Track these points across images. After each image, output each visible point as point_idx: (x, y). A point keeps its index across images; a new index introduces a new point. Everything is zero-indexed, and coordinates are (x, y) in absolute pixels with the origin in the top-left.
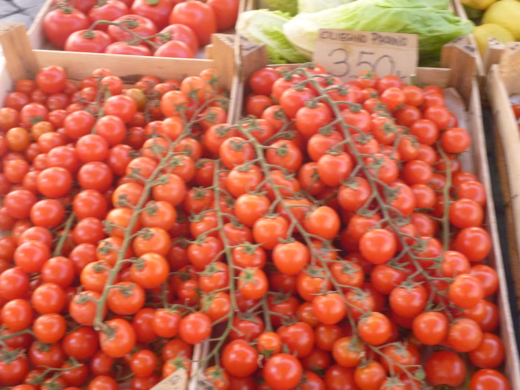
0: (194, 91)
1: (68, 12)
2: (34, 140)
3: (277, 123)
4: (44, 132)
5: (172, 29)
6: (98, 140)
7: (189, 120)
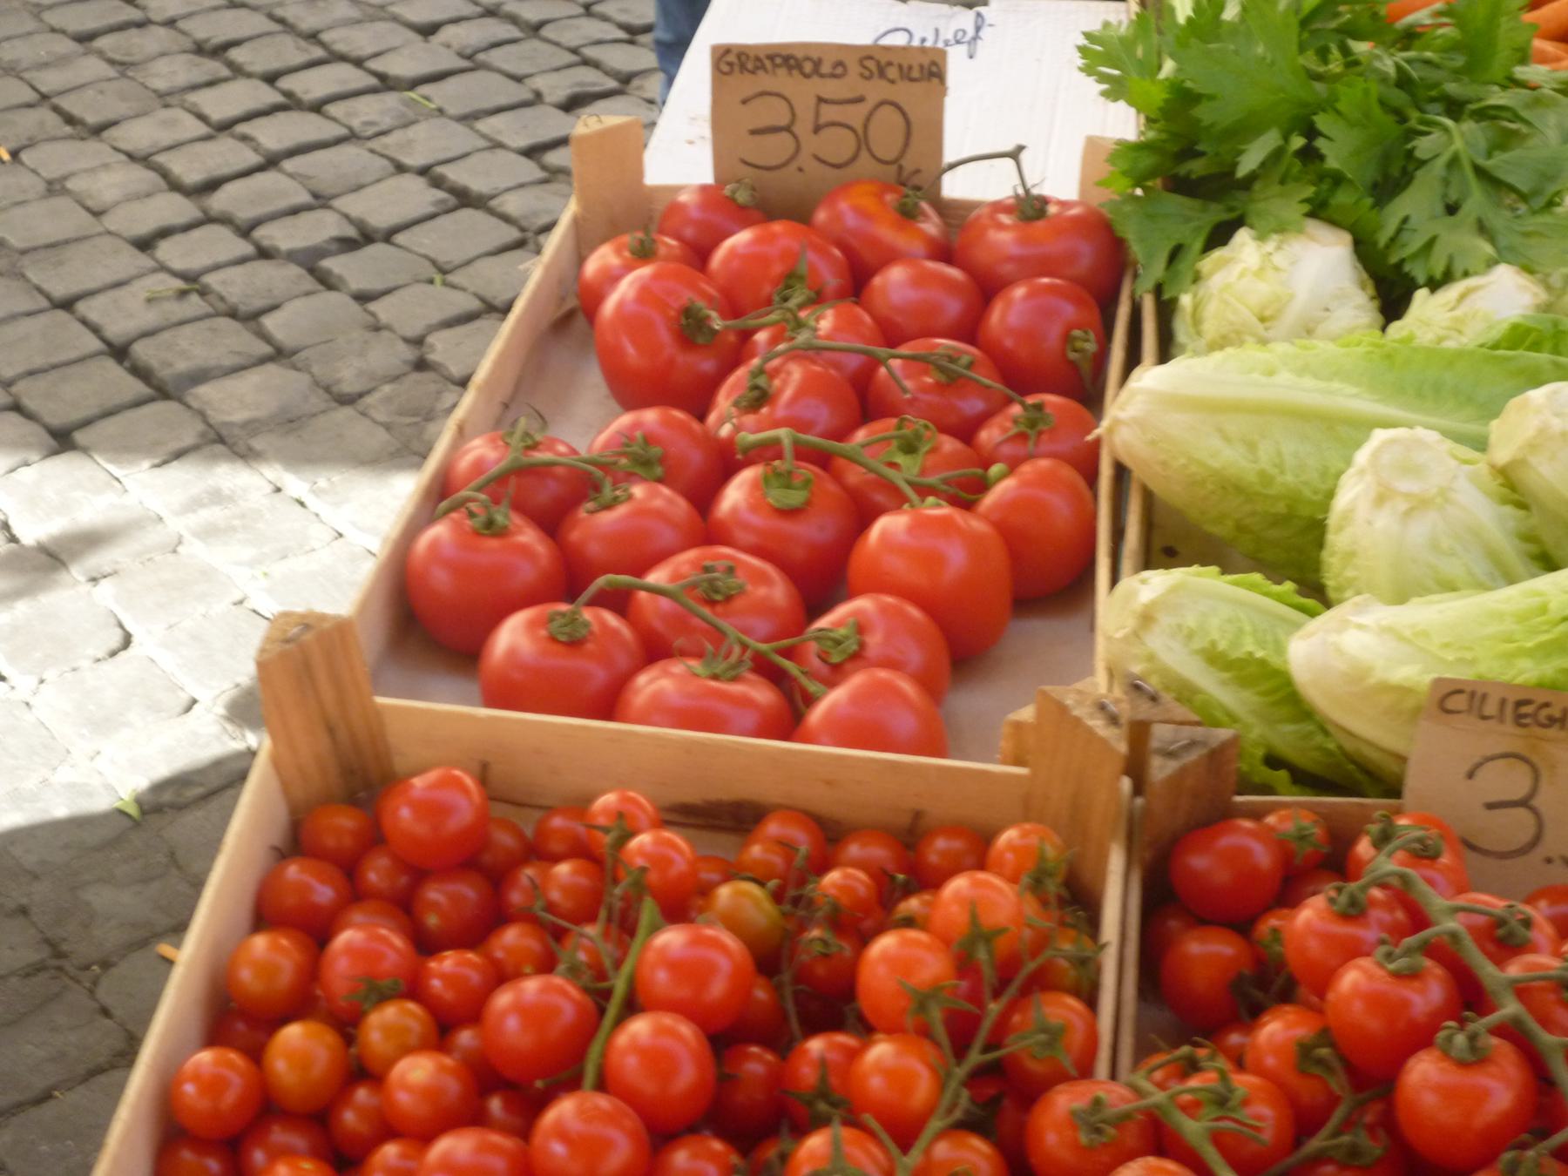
0: (979, 934)
1: (491, 528)
2: (362, 1072)
3: (1308, 1091)
4: (407, 1050)
5: (856, 613)
6: (610, 1118)
7: (960, 1052)
